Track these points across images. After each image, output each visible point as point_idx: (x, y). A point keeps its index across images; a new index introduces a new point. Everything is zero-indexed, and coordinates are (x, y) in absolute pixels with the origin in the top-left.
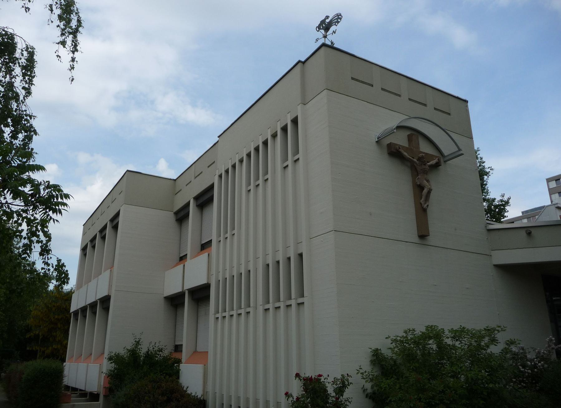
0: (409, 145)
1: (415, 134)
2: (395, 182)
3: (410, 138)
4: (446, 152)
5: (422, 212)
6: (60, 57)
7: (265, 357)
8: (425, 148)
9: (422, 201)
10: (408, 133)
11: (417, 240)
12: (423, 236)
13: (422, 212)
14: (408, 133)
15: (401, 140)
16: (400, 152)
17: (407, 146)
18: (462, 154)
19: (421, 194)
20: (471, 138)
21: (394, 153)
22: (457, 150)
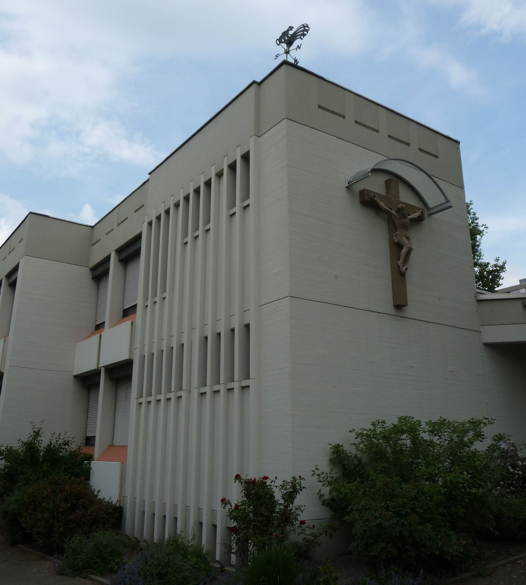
1: (394, 180)
3: (388, 184)
4: (431, 203)
5: (399, 276)
8: (405, 197)
13: (399, 276)
14: (386, 177)
15: (377, 186)
17: (384, 194)
20: (462, 187)
21: (368, 202)
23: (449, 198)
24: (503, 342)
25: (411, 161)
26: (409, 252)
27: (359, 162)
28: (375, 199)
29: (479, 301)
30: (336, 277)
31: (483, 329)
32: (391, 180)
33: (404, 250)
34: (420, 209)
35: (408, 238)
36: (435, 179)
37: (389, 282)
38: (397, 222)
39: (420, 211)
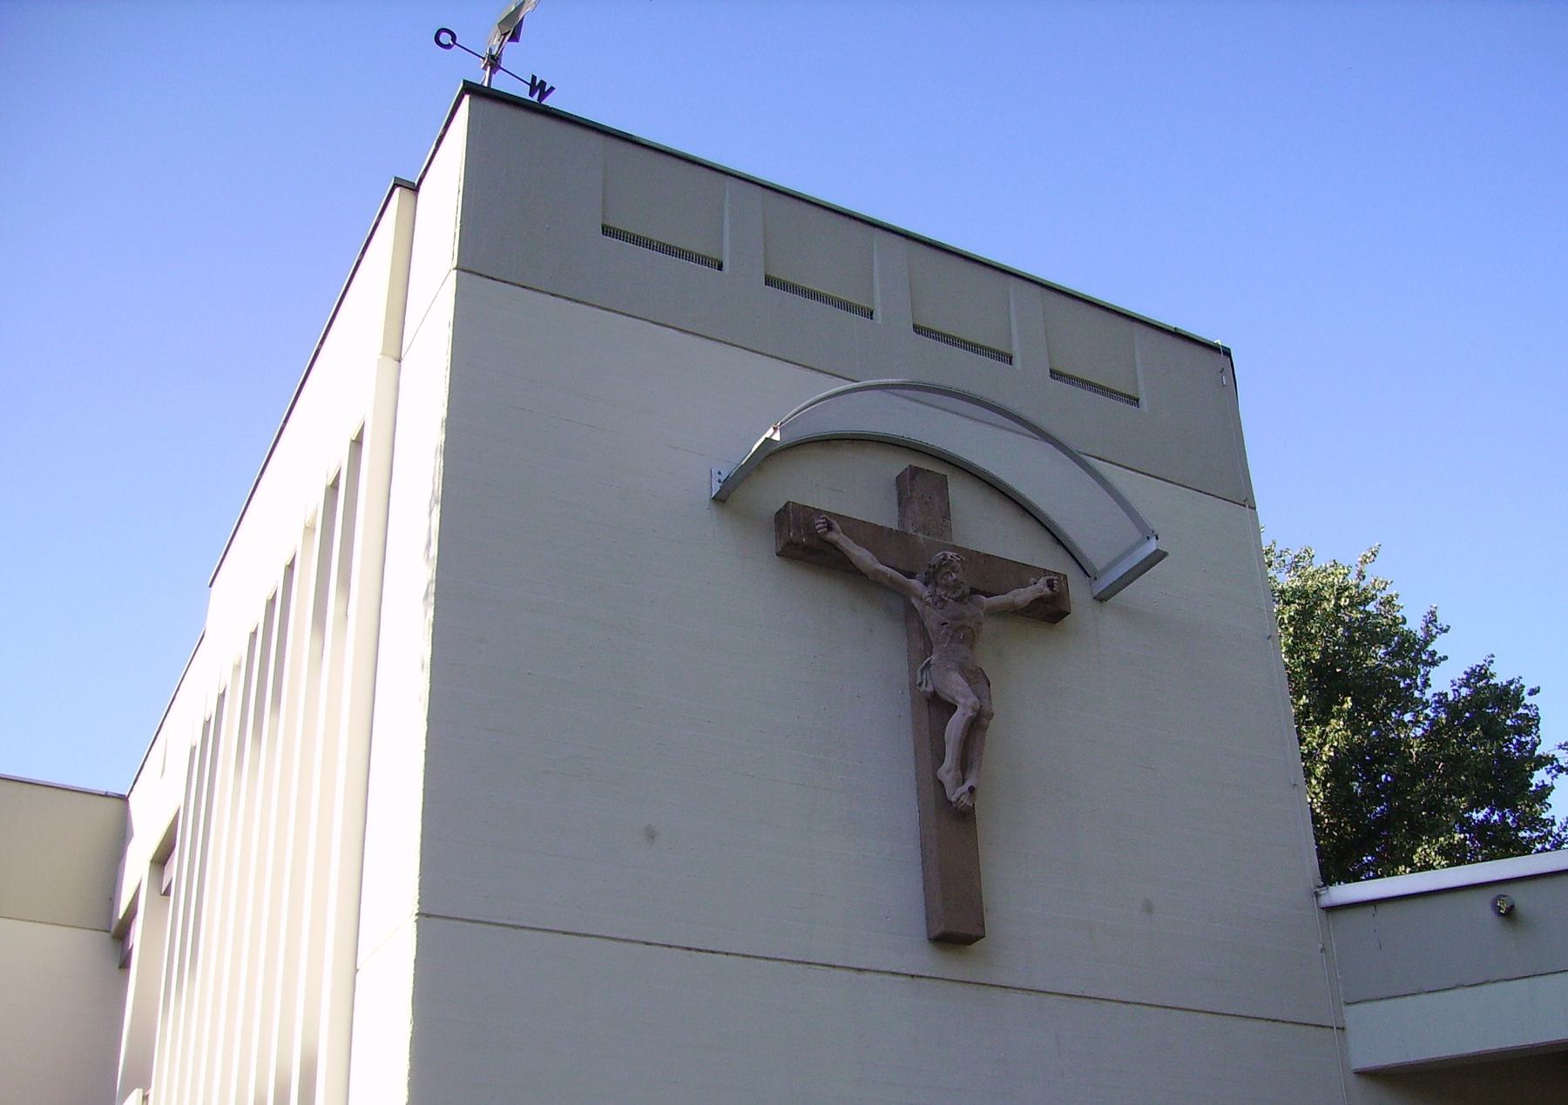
0: (901, 523)
1: (928, 473)
2: (801, 688)
3: (906, 485)
4: (1095, 550)
5: (952, 829)
6: (515, 37)
7: (176, 1019)
8: (982, 529)
9: (948, 770)
10: (897, 464)
11: (925, 959)
12: (957, 927)
13: (952, 829)
14: (897, 464)
15: (858, 494)
16: (833, 545)
17: (895, 526)
18: (1159, 556)
19: (951, 751)
20: (1248, 503)
21: (808, 544)
22: (1136, 535)
23: (1154, 523)
24: (410, 1084)
25: (1000, 401)
26: (977, 725)
27: (761, 402)
28: (833, 536)
29: (1332, 909)
30: (651, 835)
31: (1352, 1015)
32: (914, 472)
33: (955, 726)
34: (1039, 572)
35: (977, 679)
36: (1092, 461)
37: (910, 851)
38: (932, 617)
39: (1043, 580)
